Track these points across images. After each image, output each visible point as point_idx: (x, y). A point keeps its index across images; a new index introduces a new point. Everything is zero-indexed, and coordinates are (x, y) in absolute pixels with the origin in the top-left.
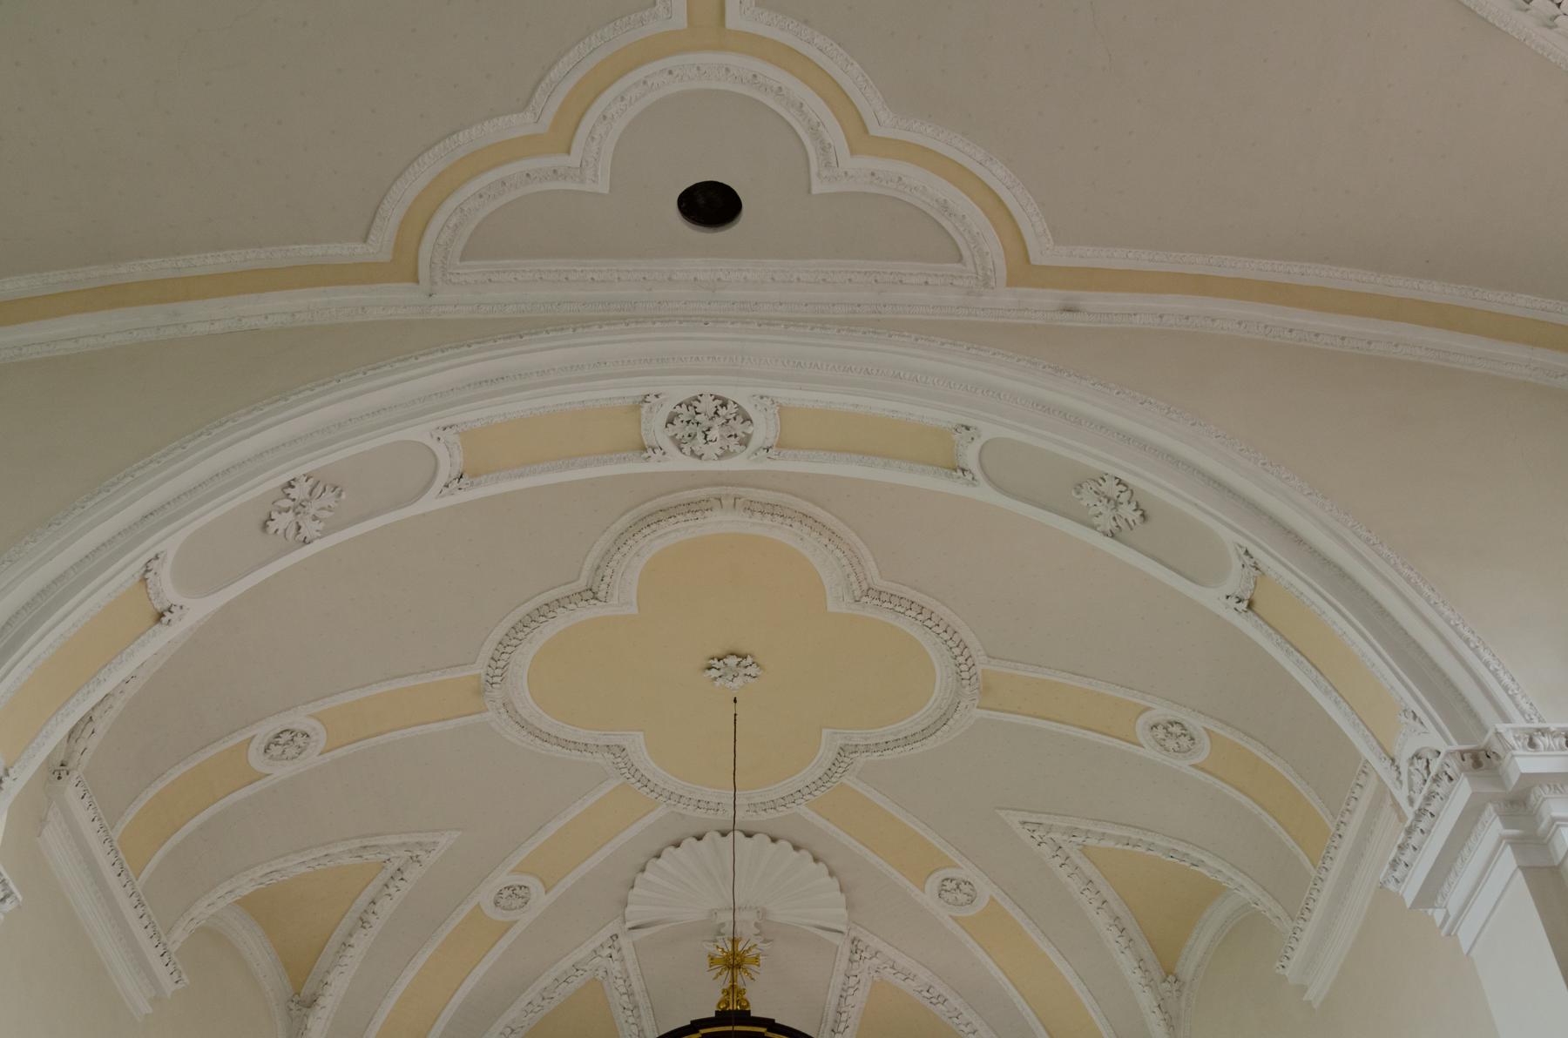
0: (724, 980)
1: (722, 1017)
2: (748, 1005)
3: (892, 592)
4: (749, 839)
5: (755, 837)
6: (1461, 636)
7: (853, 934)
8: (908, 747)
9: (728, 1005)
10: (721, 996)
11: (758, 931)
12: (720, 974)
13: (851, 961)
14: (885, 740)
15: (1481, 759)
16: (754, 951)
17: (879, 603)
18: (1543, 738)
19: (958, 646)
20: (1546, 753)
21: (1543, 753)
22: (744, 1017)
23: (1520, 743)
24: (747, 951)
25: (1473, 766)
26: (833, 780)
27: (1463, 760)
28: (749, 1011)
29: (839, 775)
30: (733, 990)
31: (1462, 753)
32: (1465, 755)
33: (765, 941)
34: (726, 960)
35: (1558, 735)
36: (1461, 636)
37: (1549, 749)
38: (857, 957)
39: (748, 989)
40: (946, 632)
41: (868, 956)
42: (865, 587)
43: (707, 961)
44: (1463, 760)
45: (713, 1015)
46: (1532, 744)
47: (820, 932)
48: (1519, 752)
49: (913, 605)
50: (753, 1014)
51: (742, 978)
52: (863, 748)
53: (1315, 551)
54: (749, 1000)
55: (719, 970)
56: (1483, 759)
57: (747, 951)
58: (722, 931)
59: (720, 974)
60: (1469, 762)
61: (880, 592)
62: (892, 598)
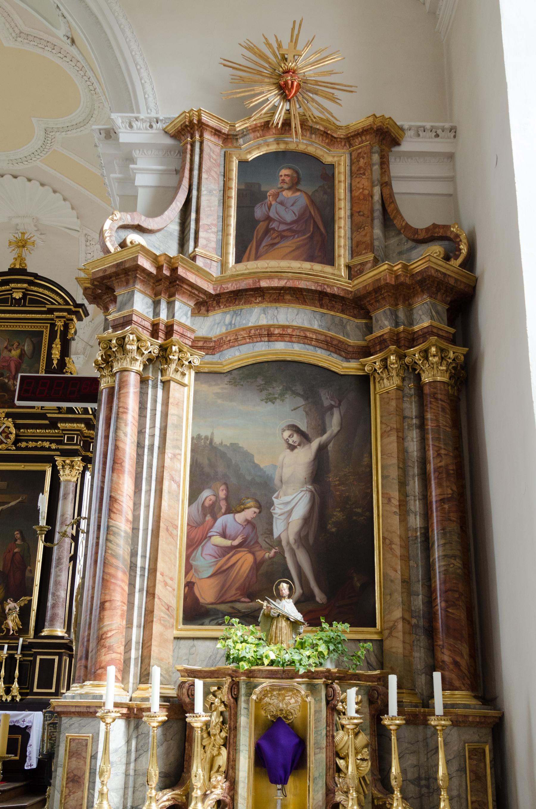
0: (14, 254)
1: (12, 271)
2: (26, 265)
3: (35, 35)
4: (14, 179)
5: (19, 178)
6: (134, 60)
7: (85, 232)
8: (78, 130)
9: (15, 266)
10: (13, 261)
11: (36, 229)
12: (14, 250)
13: (86, 246)
14: (66, 125)
15: (111, 134)
16: (32, 239)
17: (28, 42)
18: (137, 122)
19: (81, 70)
20: (138, 131)
21: (137, 131)
22: (23, 271)
23: (124, 126)
24: (29, 239)
25: (105, 137)
26: (47, 147)
27: (100, 134)
28: (26, 269)
29: (50, 145)
30: (21, 258)
31: (100, 130)
32: (102, 132)
33: (41, 234)
34: (17, 242)
35: (146, 121)
36: (134, 60)
37: (140, 129)
38: (88, 244)
39: (27, 258)
40: (71, 61)
41: (94, 244)
42: (17, 31)
43: (7, 243)
44: (100, 134)
45: (7, 270)
46: (131, 126)
47: (63, 229)
48: (123, 130)
49: (55, 47)
50: (28, 271)
51: (25, 252)
52: (56, 130)
53: (88, 7)
54: (27, 264)
55: (13, 248)
56: (112, 134)
57: (29, 239)
58: (18, 228)
59: (14, 250)
60: (103, 135)
61: (28, 35)
62: (35, 39)
